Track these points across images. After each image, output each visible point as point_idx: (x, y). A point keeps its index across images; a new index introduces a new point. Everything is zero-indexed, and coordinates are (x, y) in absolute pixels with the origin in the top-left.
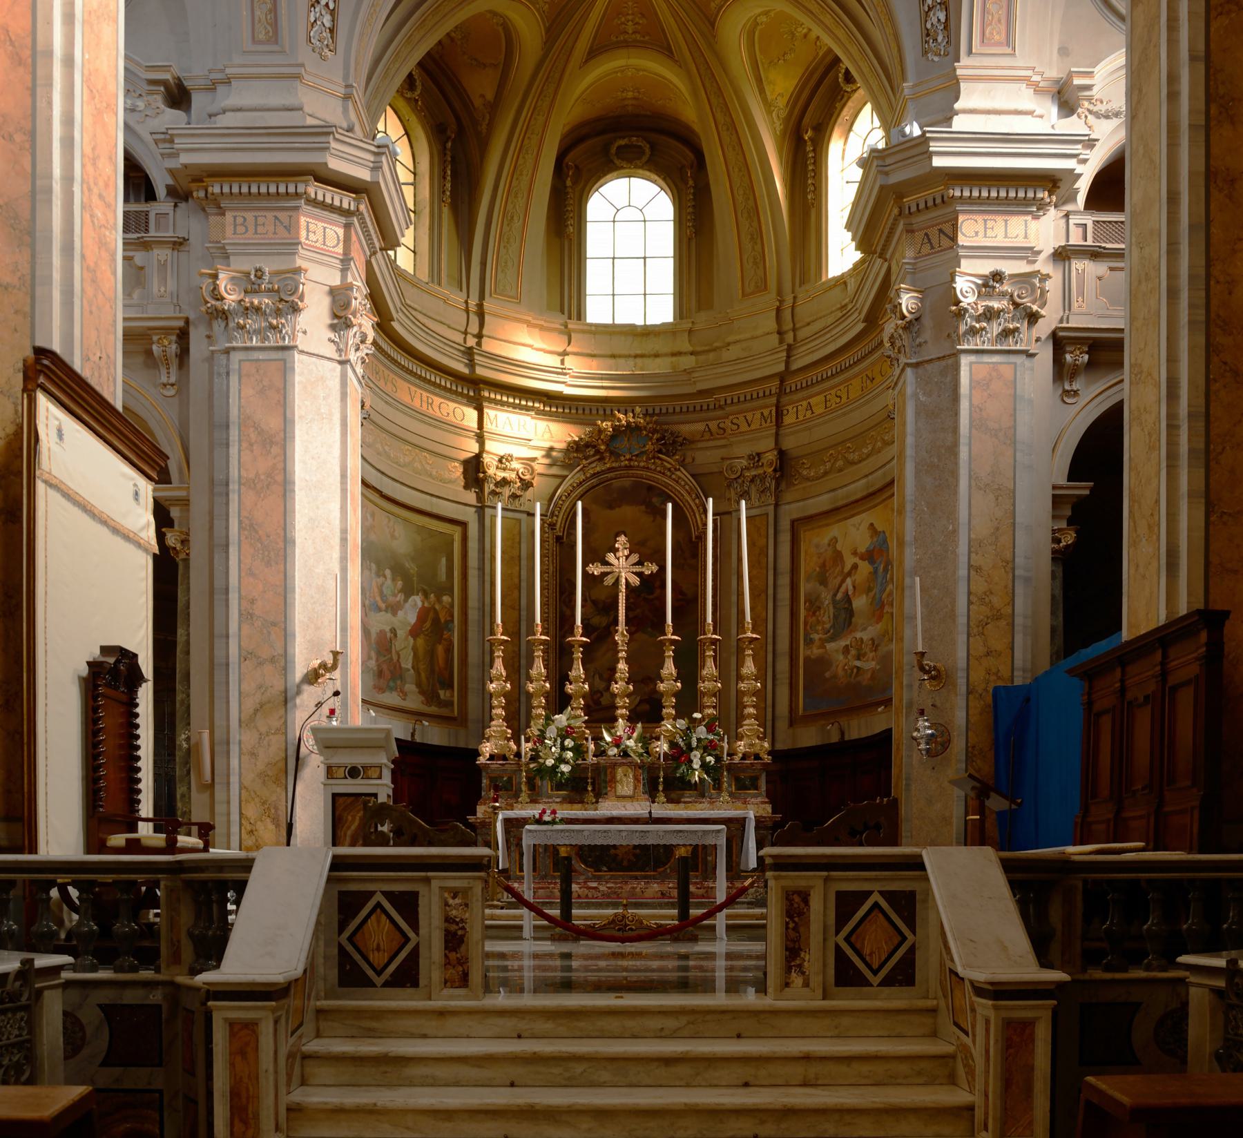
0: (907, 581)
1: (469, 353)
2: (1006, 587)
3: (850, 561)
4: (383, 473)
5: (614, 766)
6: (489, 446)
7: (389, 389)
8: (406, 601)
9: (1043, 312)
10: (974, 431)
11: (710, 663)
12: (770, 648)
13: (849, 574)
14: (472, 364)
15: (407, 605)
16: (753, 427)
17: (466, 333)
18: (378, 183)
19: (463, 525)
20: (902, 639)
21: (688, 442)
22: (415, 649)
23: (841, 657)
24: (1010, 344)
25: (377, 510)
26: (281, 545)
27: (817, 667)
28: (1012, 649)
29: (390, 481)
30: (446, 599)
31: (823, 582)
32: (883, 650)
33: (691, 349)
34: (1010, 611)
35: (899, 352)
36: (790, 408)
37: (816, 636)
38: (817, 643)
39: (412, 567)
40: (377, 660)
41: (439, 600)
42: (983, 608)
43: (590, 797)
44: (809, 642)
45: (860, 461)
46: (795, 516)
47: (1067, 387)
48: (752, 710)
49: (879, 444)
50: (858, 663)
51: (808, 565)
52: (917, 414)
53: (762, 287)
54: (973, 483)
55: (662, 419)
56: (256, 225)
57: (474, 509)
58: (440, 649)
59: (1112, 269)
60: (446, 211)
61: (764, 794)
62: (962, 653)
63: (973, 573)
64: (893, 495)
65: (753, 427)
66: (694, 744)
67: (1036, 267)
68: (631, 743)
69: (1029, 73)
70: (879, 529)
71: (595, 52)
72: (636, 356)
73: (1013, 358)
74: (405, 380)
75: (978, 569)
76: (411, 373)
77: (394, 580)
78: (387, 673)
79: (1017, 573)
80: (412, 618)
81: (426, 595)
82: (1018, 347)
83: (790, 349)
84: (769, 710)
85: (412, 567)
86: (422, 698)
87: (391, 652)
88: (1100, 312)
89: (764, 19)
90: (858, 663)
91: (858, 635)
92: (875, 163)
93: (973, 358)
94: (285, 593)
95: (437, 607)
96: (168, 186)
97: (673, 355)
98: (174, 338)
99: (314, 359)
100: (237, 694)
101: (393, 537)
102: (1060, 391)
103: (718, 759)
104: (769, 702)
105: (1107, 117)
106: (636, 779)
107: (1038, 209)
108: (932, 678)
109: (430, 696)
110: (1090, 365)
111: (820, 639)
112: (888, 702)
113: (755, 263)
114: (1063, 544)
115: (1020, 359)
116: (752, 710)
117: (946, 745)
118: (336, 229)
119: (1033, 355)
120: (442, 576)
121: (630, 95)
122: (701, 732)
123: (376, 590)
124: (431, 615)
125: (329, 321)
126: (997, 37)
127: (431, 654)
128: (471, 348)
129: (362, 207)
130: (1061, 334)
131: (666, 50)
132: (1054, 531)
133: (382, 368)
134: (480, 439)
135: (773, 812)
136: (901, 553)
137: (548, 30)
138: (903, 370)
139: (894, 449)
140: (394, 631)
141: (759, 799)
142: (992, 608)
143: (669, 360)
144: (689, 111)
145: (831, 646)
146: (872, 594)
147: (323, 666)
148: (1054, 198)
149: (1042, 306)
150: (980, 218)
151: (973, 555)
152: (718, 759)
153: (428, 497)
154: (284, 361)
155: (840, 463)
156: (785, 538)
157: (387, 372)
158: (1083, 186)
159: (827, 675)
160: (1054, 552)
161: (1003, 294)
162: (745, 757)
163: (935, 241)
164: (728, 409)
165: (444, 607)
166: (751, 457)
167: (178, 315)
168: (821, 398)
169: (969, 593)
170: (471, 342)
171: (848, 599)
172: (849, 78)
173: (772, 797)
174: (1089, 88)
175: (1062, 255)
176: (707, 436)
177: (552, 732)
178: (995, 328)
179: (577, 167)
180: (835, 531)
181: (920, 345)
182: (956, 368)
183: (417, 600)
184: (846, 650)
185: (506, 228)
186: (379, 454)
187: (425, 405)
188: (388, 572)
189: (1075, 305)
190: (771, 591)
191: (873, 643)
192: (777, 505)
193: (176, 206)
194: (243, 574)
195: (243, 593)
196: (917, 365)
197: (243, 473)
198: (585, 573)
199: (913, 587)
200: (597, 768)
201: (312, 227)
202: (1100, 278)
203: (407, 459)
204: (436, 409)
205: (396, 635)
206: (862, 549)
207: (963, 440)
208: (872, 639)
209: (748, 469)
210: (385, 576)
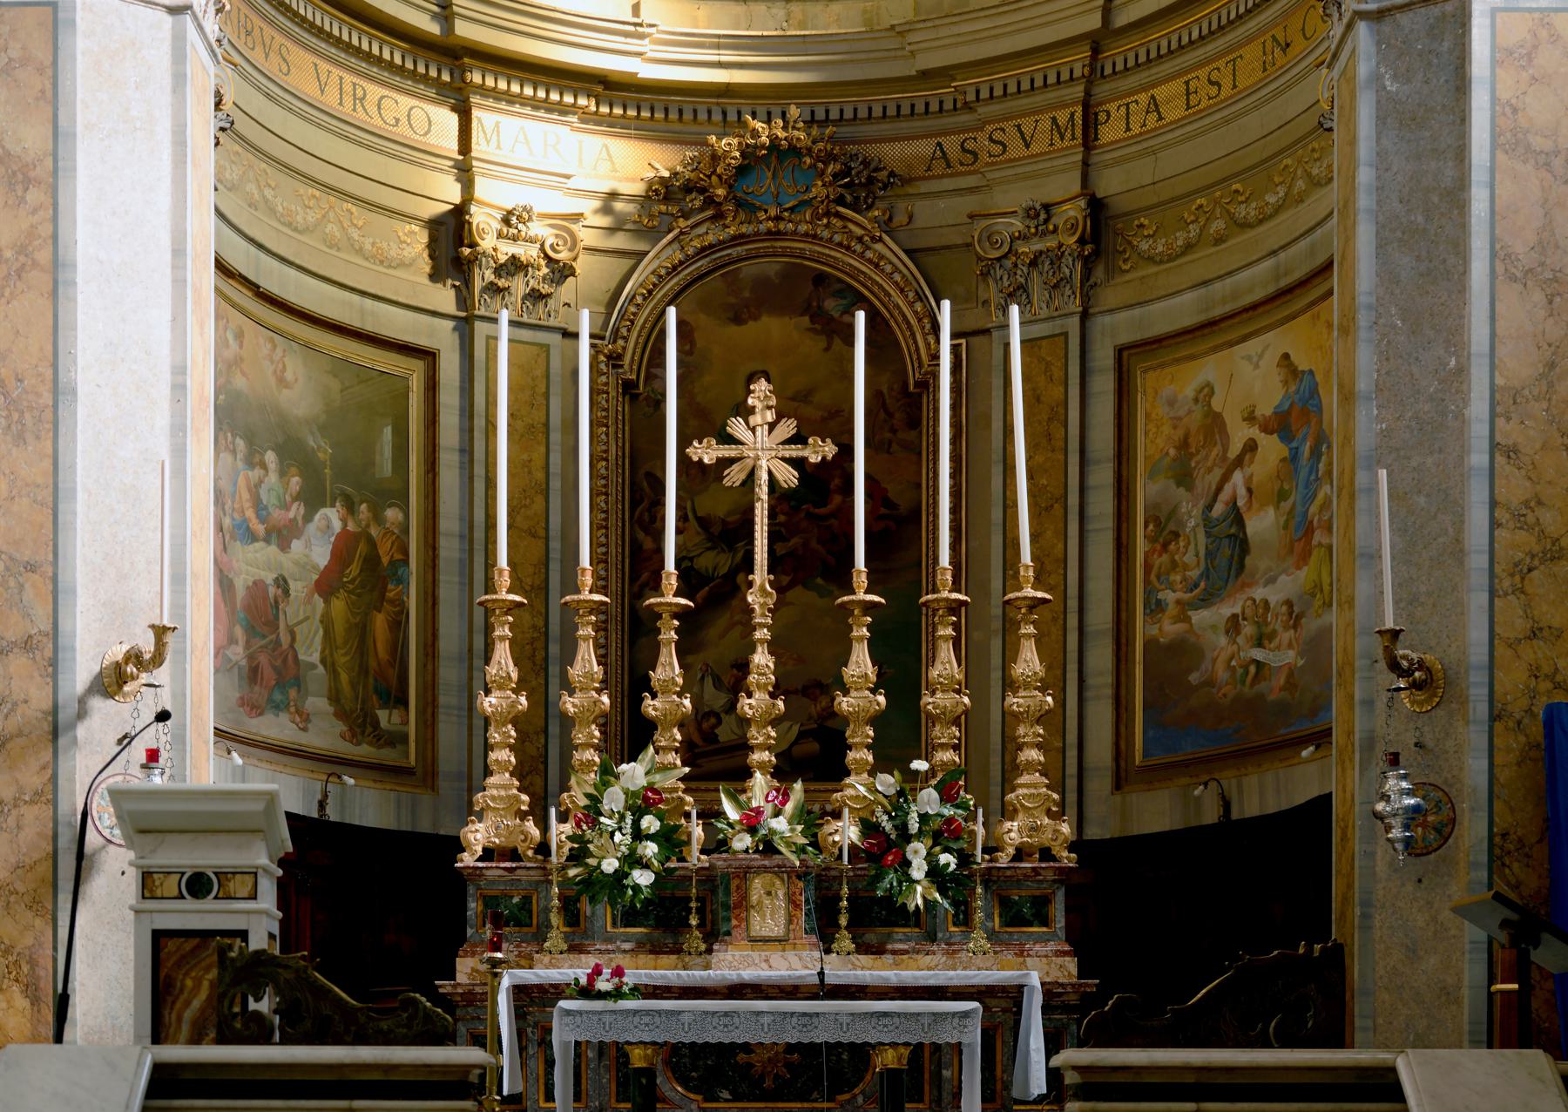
0: (1361, 478)
3: (1239, 434)
4: (260, 246)
5: (745, 873)
6: (482, 188)
7: (272, 66)
8: (308, 518)
10: (1500, 156)
11: (946, 652)
12: (1073, 621)
13: (1239, 462)
15: (312, 528)
16: (1035, 148)
19: (428, 356)
21: (898, 181)
22: (327, 622)
26: (47, 399)
29: (275, 263)
31: (1184, 478)
32: (1311, 625)
36: (1112, 107)
37: (1169, 596)
38: (1172, 610)
39: (323, 449)
40: (248, 645)
41: (378, 517)
42: (1522, 536)
43: (695, 940)
44: (1155, 608)
45: (1261, 222)
46: (1125, 338)
48: (1034, 755)
49: (1301, 184)
50: (1258, 654)
51: (1151, 442)
54: (1500, 268)
57: (450, 324)
58: (380, 622)
61: (1062, 934)
62: (1477, 634)
63: (1500, 460)
64: (1330, 293)
66: (914, 826)
68: (780, 824)
70: (1302, 364)
74: (306, 47)
75: (1511, 452)
77: (283, 473)
78: (268, 674)
80: (321, 556)
81: (350, 507)
84: (1072, 754)
85: (323, 449)
86: (341, 727)
91: (1259, 593)
101: (281, 381)
103: (965, 859)
104: (1072, 737)
106: (792, 901)
108: (1416, 686)
109: (360, 724)
112: (1321, 738)
116: (1034, 755)
117: (1445, 830)
122: (929, 800)
123: (246, 495)
124: (362, 548)
127: (361, 631)
133: (258, 21)
134: (464, 172)
136: (1348, 417)
138: (1350, 26)
139: (1331, 196)
140: (282, 583)
141: (1052, 946)
145: (1200, 617)
146: (1286, 506)
147: (134, 657)
152: (965, 859)
153: (356, 298)
155: (1218, 225)
156: (1103, 385)
157: (269, 31)
159: (1194, 678)
162: (1021, 853)
165: (388, 532)
166: (1031, 213)
168: (1177, 86)
169: (1493, 504)
173: (1080, 942)
176: (939, 167)
177: (614, 799)
180: (1208, 369)
183: (332, 517)
184: (1233, 625)
188: (270, 457)
190: (1073, 500)
192: (1085, 316)
198: (683, 460)
199: (1373, 490)
200: (708, 878)
203: (312, 217)
204: (373, 110)
205: (286, 592)
206: (1266, 409)
208: (1289, 604)
209: (1023, 237)
210: (264, 466)
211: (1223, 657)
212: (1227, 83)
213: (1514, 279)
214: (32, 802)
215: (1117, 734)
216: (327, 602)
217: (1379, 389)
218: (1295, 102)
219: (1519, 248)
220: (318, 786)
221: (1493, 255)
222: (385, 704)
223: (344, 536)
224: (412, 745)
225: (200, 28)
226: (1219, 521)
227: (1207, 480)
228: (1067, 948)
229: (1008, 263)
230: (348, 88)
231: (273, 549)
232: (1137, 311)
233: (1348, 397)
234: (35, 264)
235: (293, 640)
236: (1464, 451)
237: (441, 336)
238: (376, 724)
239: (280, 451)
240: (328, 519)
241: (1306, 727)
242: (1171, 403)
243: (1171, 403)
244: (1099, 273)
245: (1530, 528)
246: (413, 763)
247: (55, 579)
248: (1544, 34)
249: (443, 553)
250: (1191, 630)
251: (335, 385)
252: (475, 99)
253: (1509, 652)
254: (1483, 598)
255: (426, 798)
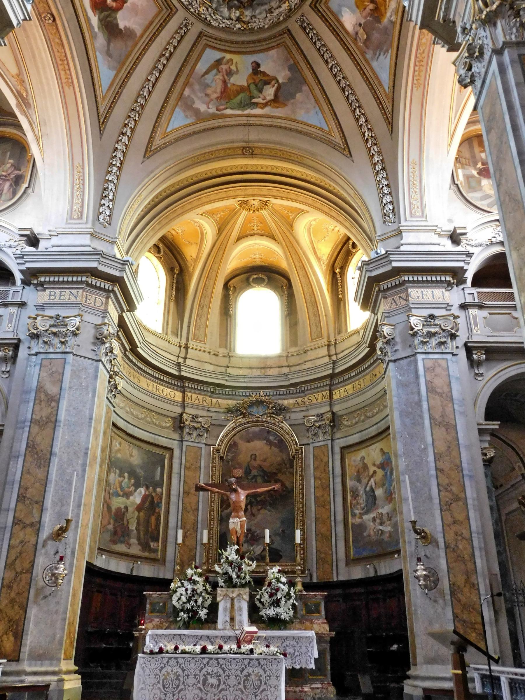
0: (401, 478)
1: (179, 365)
2: (459, 481)
3: (372, 469)
4: (128, 422)
6: (187, 410)
7: (136, 381)
8: (135, 491)
9: (457, 334)
10: (429, 394)
13: (372, 476)
14: (180, 370)
15: (136, 493)
16: (319, 401)
17: (178, 357)
18: (123, 277)
19: (171, 450)
20: (401, 513)
22: (138, 518)
23: (372, 524)
24: (443, 349)
25: (123, 442)
26: (48, 456)
27: (360, 528)
28: (469, 519)
29: (132, 426)
30: (159, 490)
31: (359, 480)
32: (394, 520)
33: (287, 365)
34: (463, 496)
35: (385, 355)
36: (336, 391)
37: (357, 512)
38: (358, 515)
39: (140, 472)
40: (114, 525)
41: (155, 490)
42: (447, 494)
44: (354, 515)
45: (373, 416)
46: (342, 445)
47: (477, 372)
49: (382, 407)
50: (381, 528)
52: (398, 386)
53: (320, 336)
54: (432, 422)
55: (273, 397)
56: (60, 295)
57: (177, 442)
58: (153, 519)
59: (490, 314)
60: (172, 304)
61: (324, 616)
62: (439, 522)
63: (439, 473)
64: (390, 434)
65: (319, 401)
67: (451, 312)
69: (435, 228)
70: (386, 451)
71: (239, 239)
72: (261, 368)
73: (445, 356)
74: (145, 377)
75: (441, 470)
76: (148, 374)
77: (129, 479)
78: (120, 533)
79: (464, 473)
80: (138, 500)
81: (147, 488)
82: (447, 351)
83: (334, 363)
84: (334, 555)
86: (139, 547)
87: (123, 520)
88: (488, 334)
89: (313, 223)
90: (381, 528)
91: (380, 511)
92: (365, 267)
93: (424, 356)
94: (46, 484)
95: (153, 494)
96: (21, 279)
97: (279, 367)
98: (11, 349)
99: (82, 359)
100: (7, 547)
101: (131, 456)
102: (473, 374)
105: (476, 246)
107: (448, 286)
108: (423, 538)
109: (145, 547)
110: (487, 359)
111: (360, 513)
112: (398, 552)
113: (316, 325)
114: (488, 456)
115: (449, 357)
117: (436, 582)
118: (102, 299)
119: (456, 355)
120: (158, 477)
121: (257, 256)
123: (118, 485)
124: (150, 499)
125: (92, 341)
126: (418, 214)
127: (148, 522)
128: (179, 363)
129: (116, 289)
130: (469, 344)
131: (273, 238)
132: (482, 449)
133: (132, 371)
134: (184, 407)
135: (330, 631)
136: (397, 461)
137: (219, 229)
138: (388, 364)
139: (388, 411)
140: (126, 508)
141: (321, 621)
142: (453, 494)
143: (277, 369)
144: (284, 264)
145: (365, 517)
146: (385, 487)
147: (61, 529)
148: (455, 281)
149: (457, 331)
150: (419, 290)
151: (438, 462)
153: (153, 436)
154: (65, 359)
155: (363, 418)
156: (338, 457)
157: (135, 373)
158: (469, 276)
159: (365, 534)
160: (484, 461)
161: (436, 325)
163: (398, 302)
164: (306, 392)
165: (157, 494)
166: (318, 416)
167: (15, 337)
168: (351, 386)
169: (438, 485)
170: (181, 360)
171: (372, 490)
172: (354, 245)
173: (330, 619)
174: (464, 234)
175: (464, 307)
176: (296, 406)
178: (434, 341)
179: (234, 287)
180: (363, 453)
181: (396, 351)
182: (416, 361)
184: (374, 519)
185: (200, 311)
186: (127, 413)
187: (155, 390)
188: (126, 475)
189: (474, 331)
191: (388, 516)
193: (24, 288)
194: (24, 473)
195: (22, 484)
196: (395, 361)
197: (34, 416)
199: (404, 481)
201: (89, 297)
202: (485, 318)
203: (143, 416)
204: (161, 392)
205: (127, 510)
206: (378, 463)
207: (424, 398)
208: (388, 514)
209: (316, 421)
210: (124, 477)
211: (373, 528)
212: (362, 385)
213: (436, 425)
214: (25, 573)
215: (346, 550)
216: (139, 513)
217: (404, 454)
218: (379, 388)
219: (437, 417)
220: (132, 564)
221: (430, 418)
222: (152, 541)
223: (145, 495)
224: (159, 553)
225: (104, 366)
226: (369, 492)
227: (364, 481)
228: (326, 621)
229: (313, 428)
230: (155, 386)
231: (124, 499)
232: (345, 439)
233: (396, 456)
234: (51, 421)
235: (128, 523)
236: (429, 471)
237: (175, 445)
238: (150, 546)
239: (129, 473)
240: (141, 491)
241: (395, 549)
242: (355, 461)
243: (355, 461)
244: (335, 430)
245: (449, 491)
246: (159, 557)
247: (42, 506)
248: (436, 364)
249: (171, 500)
250: (363, 521)
251: (146, 456)
252: (186, 389)
253: (448, 528)
254: (439, 512)
255: (162, 568)
